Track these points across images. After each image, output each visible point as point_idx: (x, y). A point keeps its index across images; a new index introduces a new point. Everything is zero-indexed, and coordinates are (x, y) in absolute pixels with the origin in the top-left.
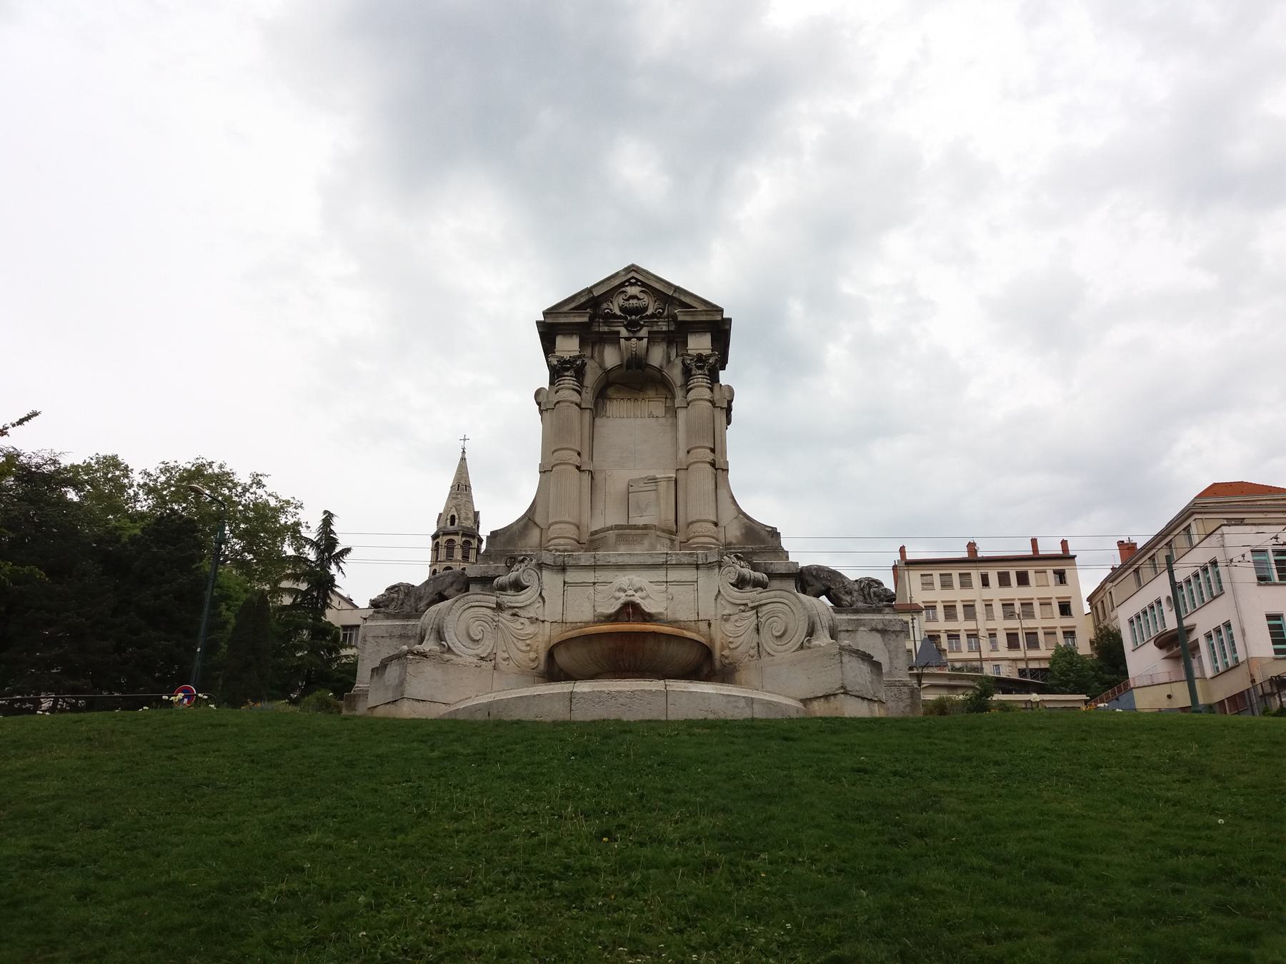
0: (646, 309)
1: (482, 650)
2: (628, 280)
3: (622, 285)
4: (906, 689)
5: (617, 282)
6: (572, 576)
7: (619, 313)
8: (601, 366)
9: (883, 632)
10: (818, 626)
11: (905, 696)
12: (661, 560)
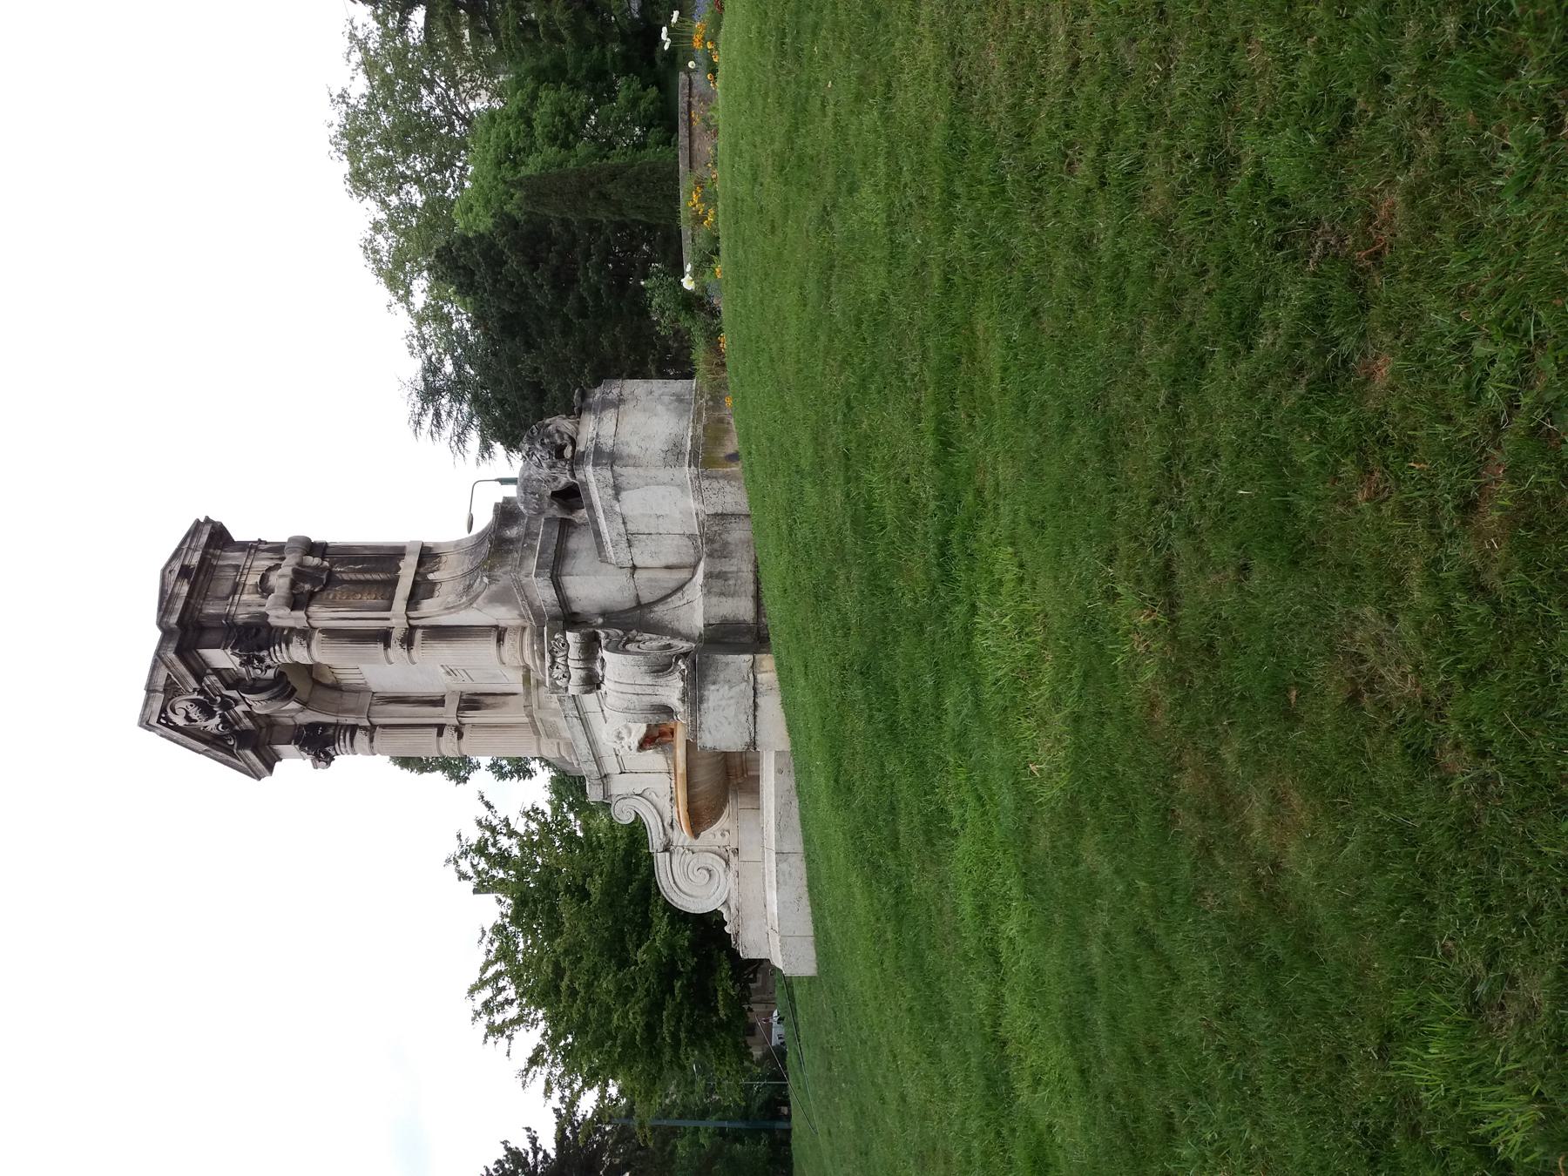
3: (176, 728)
4: (705, 484)
5: (177, 735)
7: (217, 720)
9: (617, 490)
10: (656, 700)
11: (715, 485)
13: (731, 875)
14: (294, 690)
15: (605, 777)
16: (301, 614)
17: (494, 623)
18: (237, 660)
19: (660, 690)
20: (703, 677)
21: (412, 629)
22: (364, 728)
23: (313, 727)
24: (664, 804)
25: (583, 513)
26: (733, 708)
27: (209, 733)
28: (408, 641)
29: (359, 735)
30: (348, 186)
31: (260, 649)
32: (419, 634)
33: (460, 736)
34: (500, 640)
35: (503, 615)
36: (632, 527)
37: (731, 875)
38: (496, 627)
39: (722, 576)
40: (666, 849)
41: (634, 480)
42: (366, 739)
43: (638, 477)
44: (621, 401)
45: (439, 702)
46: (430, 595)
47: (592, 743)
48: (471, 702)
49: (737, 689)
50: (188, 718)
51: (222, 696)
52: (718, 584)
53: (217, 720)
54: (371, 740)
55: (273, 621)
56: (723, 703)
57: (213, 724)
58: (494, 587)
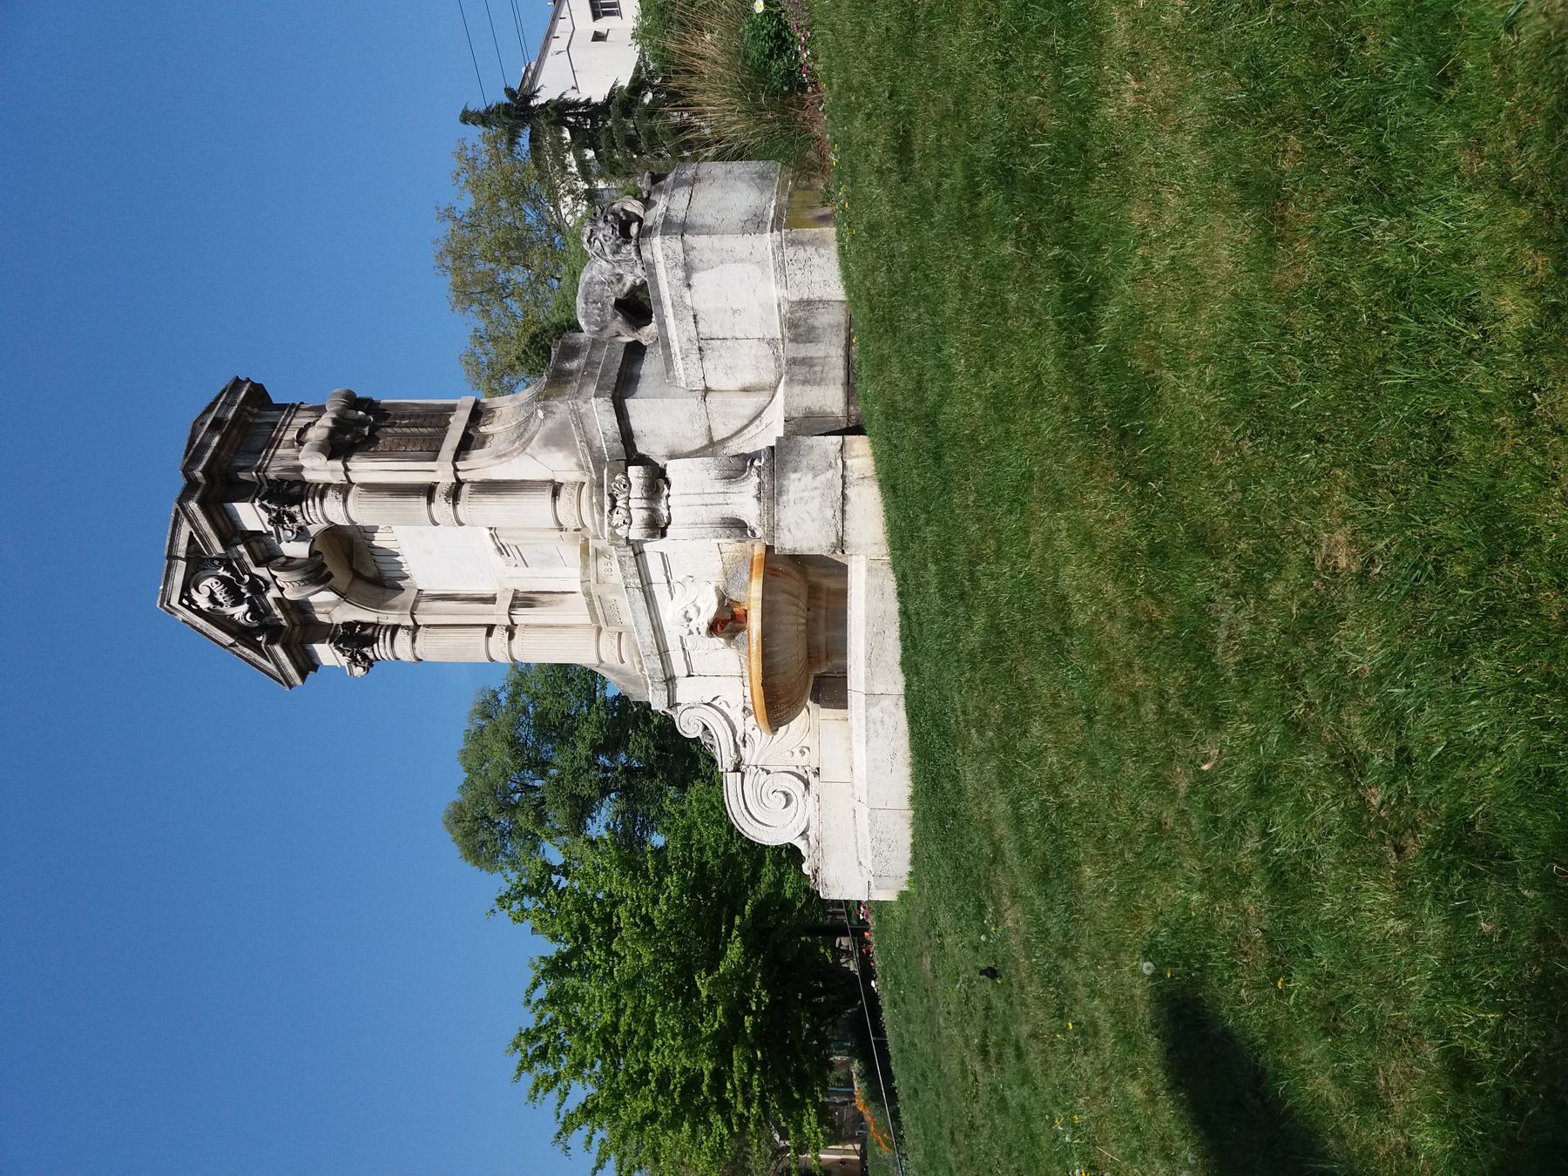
0: (222, 579)
1: (796, 787)
2: (188, 608)
4: (789, 252)
6: (679, 669)
7: (245, 607)
8: (336, 604)
9: (689, 269)
11: (802, 254)
12: (639, 595)
13: (811, 799)
14: (330, 576)
15: (670, 681)
16: (338, 464)
17: (549, 477)
18: (265, 516)
19: (732, 498)
20: (784, 464)
21: (459, 483)
22: (407, 628)
23: (349, 626)
24: (736, 715)
25: (652, 328)
26: (818, 501)
27: (236, 623)
28: (454, 494)
29: (401, 633)
30: (452, 295)
31: (291, 505)
32: (466, 489)
33: (511, 637)
34: (555, 494)
35: (561, 465)
36: (705, 329)
37: (811, 799)
38: (552, 482)
39: (806, 362)
40: (737, 769)
41: (707, 255)
42: (408, 639)
43: (712, 250)
44: (695, 180)
45: (491, 600)
46: (482, 445)
47: (657, 629)
48: (522, 600)
49: (822, 478)
50: (212, 598)
51: (251, 575)
52: (801, 372)
53: (245, 607)
54: (414, 640)
55: (309, 476)
56: (806, 495)
57: (240, 612)
58: (550, 424)
